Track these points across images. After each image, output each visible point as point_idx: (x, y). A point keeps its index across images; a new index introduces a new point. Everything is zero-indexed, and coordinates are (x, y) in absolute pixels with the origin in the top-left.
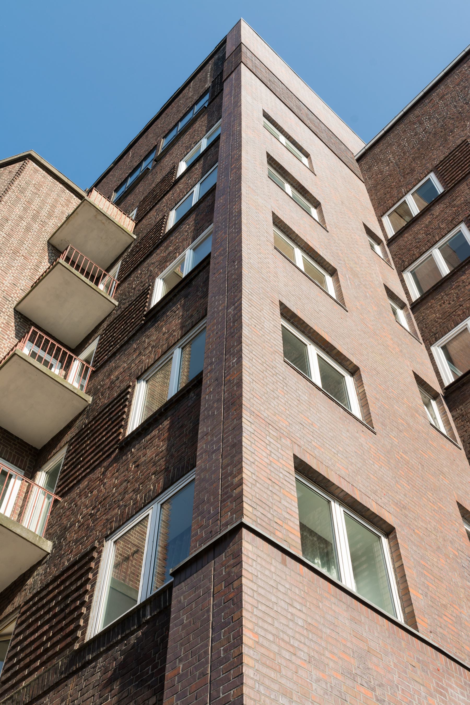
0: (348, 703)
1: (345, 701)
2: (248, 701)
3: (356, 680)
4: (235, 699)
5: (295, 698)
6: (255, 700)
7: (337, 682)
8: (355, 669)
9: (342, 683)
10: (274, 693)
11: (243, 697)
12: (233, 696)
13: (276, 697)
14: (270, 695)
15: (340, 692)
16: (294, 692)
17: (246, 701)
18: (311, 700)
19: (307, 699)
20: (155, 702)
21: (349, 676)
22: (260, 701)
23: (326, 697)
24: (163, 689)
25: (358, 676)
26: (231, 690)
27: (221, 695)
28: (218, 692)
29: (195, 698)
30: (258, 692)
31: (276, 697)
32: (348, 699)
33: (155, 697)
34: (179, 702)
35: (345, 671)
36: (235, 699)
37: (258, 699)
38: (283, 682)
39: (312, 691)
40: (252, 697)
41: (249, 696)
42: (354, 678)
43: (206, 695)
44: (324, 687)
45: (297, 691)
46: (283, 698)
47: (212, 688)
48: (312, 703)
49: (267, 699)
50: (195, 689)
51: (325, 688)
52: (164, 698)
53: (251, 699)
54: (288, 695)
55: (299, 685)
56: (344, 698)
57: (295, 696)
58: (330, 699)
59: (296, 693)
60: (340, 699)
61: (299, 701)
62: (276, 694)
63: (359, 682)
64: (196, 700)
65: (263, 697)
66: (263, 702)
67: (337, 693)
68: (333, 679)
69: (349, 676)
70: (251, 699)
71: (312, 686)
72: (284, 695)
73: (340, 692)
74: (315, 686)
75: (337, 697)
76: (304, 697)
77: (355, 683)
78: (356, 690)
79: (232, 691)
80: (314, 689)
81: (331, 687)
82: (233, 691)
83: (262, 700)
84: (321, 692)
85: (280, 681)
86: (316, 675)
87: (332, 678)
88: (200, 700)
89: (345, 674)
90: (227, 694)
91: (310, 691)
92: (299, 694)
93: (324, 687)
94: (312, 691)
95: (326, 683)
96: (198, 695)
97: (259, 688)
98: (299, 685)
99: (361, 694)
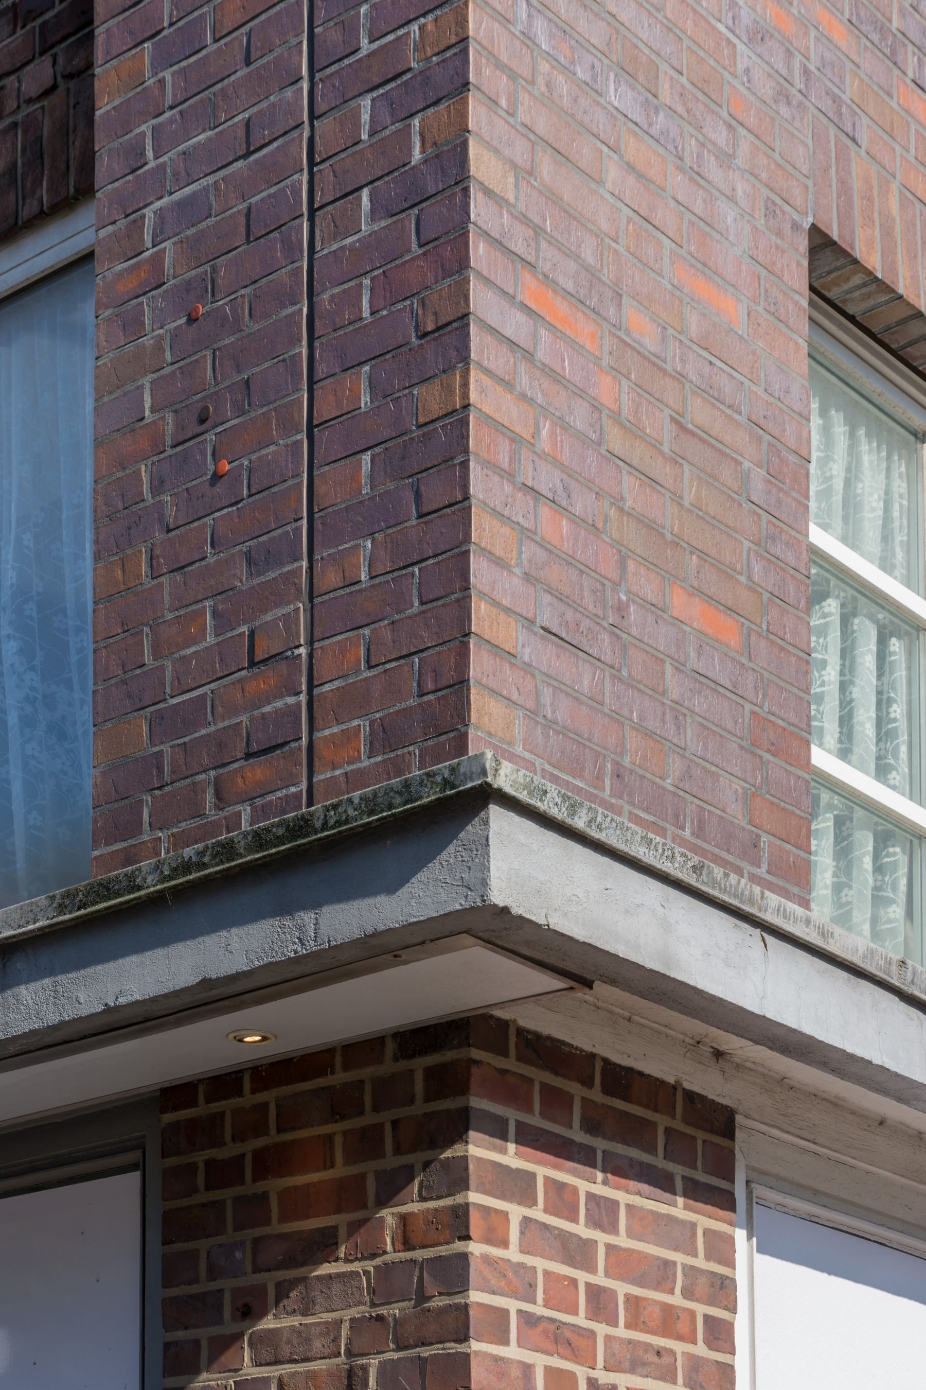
0: (863, 153)
1: (849, 143)
2: (487, 72)
3: (899, 59)
4: (428, 59)
5: (666, 94)
6: (513, 76)
7: (828, 55)
8: (903, 14)
9: (849, 65)
10: (589, 59)
11: (465, 51)
12: (420, 47)
13: (594, 78)
14: (573, 62)
15: (836, 99)
16: (664, 67)
17: (479, 73)
18: (725, 114)
19: (713, 106)
20: (48, 83)
21: (875, 37)
22: (533, 83)
23: (784, 110)
24: (91, 22)
25: (910, 47)
26: (409, 22)
27: (364, 42)
28: (350, 29)
29: (240, 56)
30: (528, 38)
31: (594, 78)
32: (863, 138)
33: (47, 59)
34: (167, 75)
35: (862, 13)
36: (428, 59)
37: (525, 72)
38: (624, 17)
39: (734, 75)
40: (504, 58)
41: (490, 53)
42: (894, 52)
43: (294, 41)
44: (781, 66)
45: (676, 63)
46: (623, 88)
47: (320, 15)
48: (730, 126)
49: (561, 79)
50: (240, 18)
51: (784, 72)
52: (99, 55)
53: (499, 65)
54: (641, 78)
55: (686, 42)
56: (849, 129)
57: (667, 86)
58: (797, 123)
59: (672, 72)
60: (833, 131)
61: (680, 109)
62: (597, 64)
63: (910, 74)
64: (248, 63)
65: (544, 67)
66: (543, 88)
67: (827, 104)
68: (817, 39)
69: (875, 37)
70: (499, 65)
71: (734, 55)
72: (627, 72)
73: (836, 99)
74: (745, 55)
75: (825, 121)
76: (700, 95)
77: (896, 72)
78: (894, 104)
79: (415, 27)
80: (740, 68)
81: (806, 72)
82: (422, 28)
83: (540, 81)
84: (767, 89)
85: (614, 11)
86: (755, 11)
87: (813, 33)
88: (263, 66)
89: (864, 28)
90: (391, 37)
91: (726, 74)
92: (683, 80)
93: (781, 66)
94: (734, 75)
95: (789, 54)
96: (256, 43)
97: (530, 24)
98: (686, 42)
99: (913, 126)
